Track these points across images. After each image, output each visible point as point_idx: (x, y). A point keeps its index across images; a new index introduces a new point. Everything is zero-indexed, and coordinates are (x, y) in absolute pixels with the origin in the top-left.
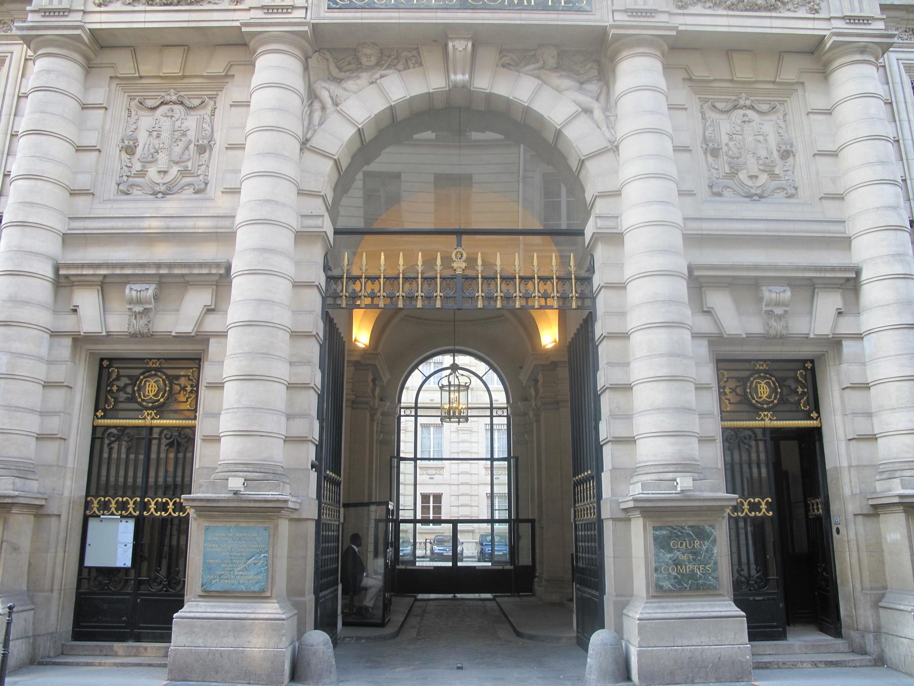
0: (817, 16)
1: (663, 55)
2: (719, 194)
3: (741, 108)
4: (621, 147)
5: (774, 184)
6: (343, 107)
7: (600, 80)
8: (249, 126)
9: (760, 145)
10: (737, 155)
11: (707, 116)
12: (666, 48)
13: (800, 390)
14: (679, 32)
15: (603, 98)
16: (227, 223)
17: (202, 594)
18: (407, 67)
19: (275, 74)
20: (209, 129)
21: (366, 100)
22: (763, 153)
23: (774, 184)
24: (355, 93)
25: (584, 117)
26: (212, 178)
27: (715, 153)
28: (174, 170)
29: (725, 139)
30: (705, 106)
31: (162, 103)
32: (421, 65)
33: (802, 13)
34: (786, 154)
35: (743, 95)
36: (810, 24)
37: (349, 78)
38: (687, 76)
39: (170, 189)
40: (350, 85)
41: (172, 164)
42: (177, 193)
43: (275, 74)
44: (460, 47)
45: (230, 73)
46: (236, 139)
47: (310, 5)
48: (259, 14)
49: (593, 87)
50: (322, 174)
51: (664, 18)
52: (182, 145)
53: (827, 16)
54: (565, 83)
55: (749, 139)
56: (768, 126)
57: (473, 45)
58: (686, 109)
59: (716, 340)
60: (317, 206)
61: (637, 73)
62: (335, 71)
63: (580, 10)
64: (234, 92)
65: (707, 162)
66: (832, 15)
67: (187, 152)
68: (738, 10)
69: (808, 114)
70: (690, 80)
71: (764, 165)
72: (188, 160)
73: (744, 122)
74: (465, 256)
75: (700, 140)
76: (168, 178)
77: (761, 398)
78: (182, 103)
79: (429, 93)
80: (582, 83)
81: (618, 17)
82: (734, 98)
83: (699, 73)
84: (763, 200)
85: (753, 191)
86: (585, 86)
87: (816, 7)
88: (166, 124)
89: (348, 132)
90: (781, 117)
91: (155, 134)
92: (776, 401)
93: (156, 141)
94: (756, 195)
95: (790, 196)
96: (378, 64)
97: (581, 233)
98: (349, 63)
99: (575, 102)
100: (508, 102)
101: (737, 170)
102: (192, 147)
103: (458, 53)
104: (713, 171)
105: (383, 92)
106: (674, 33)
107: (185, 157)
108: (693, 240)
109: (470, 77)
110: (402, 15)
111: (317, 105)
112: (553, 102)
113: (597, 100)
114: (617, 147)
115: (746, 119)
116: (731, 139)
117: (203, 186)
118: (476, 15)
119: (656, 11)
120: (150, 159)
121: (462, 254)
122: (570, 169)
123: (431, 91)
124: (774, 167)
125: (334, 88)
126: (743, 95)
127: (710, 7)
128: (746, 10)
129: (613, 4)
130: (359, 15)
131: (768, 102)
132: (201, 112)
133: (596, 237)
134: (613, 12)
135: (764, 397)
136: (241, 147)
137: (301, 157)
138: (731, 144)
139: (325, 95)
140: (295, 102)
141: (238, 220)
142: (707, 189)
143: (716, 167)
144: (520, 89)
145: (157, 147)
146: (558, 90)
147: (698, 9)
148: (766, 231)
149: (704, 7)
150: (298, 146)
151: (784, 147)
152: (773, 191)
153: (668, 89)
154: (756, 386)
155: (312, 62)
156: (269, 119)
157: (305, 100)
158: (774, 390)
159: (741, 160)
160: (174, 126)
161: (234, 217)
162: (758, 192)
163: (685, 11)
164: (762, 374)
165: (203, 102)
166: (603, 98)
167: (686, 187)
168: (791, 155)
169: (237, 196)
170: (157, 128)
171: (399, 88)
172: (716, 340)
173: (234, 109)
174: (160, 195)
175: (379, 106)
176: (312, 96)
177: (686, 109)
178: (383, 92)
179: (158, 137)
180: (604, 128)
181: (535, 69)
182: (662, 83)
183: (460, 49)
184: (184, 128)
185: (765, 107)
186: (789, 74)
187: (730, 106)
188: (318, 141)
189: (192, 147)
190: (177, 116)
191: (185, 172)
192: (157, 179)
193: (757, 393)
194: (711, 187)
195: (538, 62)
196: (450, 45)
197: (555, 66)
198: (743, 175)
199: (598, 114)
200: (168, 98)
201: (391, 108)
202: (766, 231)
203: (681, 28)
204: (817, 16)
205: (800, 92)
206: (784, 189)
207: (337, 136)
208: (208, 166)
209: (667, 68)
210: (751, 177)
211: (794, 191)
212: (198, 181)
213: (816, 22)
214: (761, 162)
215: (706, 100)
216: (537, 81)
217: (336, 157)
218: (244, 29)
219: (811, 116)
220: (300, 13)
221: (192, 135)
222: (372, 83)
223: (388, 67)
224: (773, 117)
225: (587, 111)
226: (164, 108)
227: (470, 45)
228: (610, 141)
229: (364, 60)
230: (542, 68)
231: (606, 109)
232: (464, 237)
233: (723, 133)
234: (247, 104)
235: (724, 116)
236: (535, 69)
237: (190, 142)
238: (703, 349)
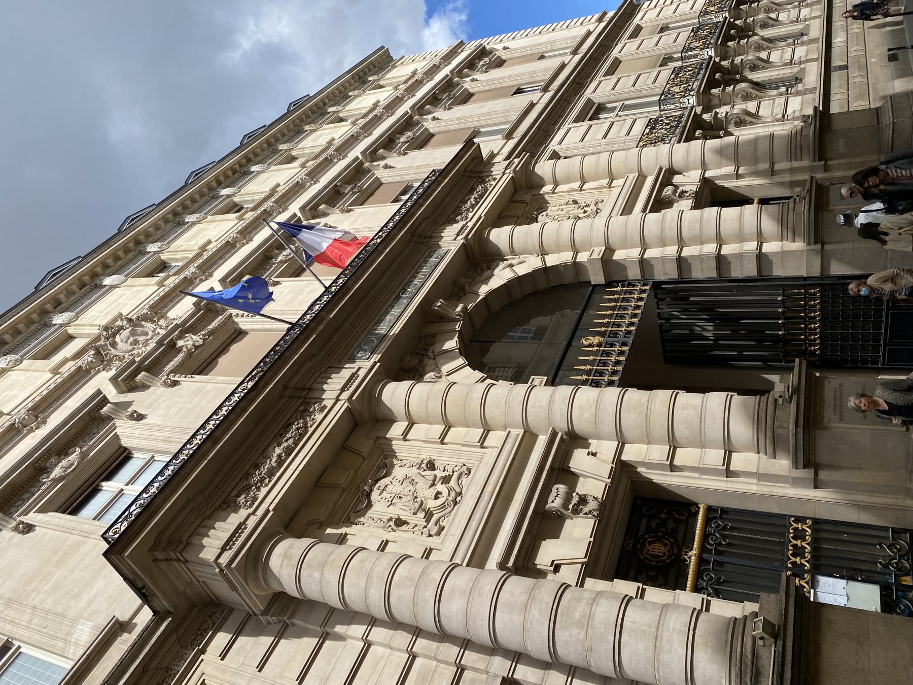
3: (371, 490)
5: (453, 482)
13: (663, 516)
17: (21, 650)
27: (400, 523)
38: (317, 525)
56: (398, 472)
59: (594, 567)
77: (664, 553)
82: (359, 494)
92: (672, 540)
95: (469, 470)
104: (416, 529)
106: (271, 513)
127: (270, 481)
135: (663, 550)
151: (424, 466)
154: (651, 555)
158: (659, 540)
162: (453, 494)
163: (259, 500)
164: (639, 546)
172: (594, 567)
182: (306, 542)
193: (660, 556)
194: (430, 535)
210: (436, 498)
238: (593, 584)
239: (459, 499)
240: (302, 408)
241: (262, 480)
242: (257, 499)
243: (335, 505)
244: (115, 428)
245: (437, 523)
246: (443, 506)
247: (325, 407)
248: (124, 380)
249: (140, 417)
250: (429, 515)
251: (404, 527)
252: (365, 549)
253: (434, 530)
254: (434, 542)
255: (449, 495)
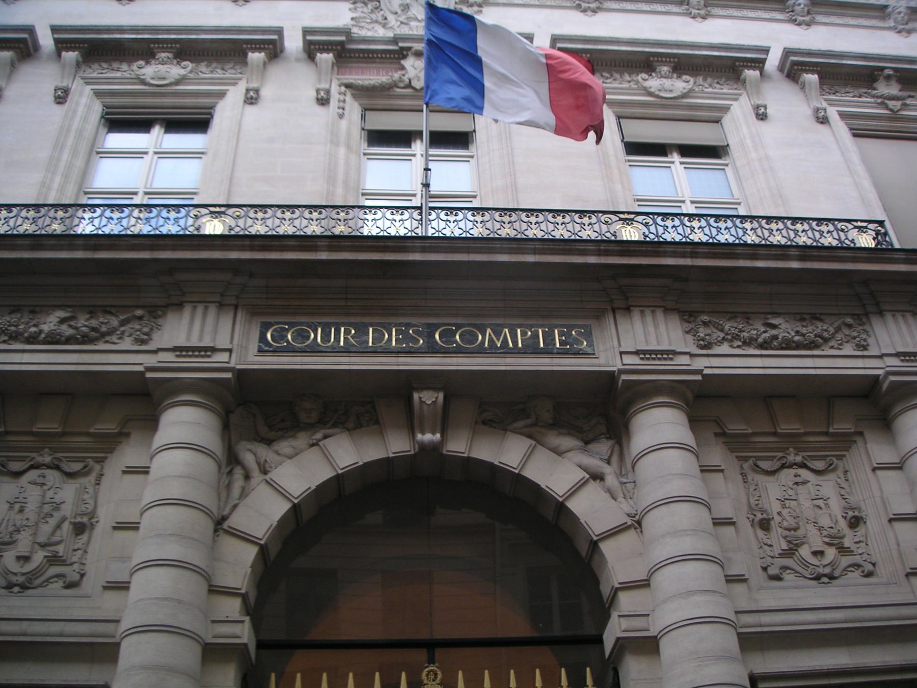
0: (866, 353)
1: (687, 405)
2: (777, 578)
3: (790, 467)
4: (644, 524)
5: (845, 561)
6: (273, 475)
7: (609, 438)
8: (147, 498)
9: (820, 512)
10: (794, 525)
11: (750, 478)
12: (690, 396)
14: (705, 376)
15: (615, 459)
16: (109, 628)
18: (359, 426)
19: (185, 425)
20: (92, 502)
21: (301, 470)
22: (825, 522)
23: (845, 561)
24: (290, 458)
25: (593, 486)
26: (90, 569)
27: (765, 525)
28: (39, 557)
29: (776, 507)
30: (746, 465)
31: (32, 467)
32: (377, 422)
33: (848, 350)
34: (855, 522)
35: (791, 449)
36: (859, 363)
37: (282, 438)
38: (719, 431)
39: (30, 581)
40: (285, 446)
41: (37, 547)
42: (40, 586)
43: (185, 425)
44: (428, 398)
45: (125, 431)
46: (130, 515)
47: (235, 347)
48: (170, 357)
49: (604, 447)
50: (238, 565)
51: (683, 361)
52: (53, 522)
53: (878, 353)
54: (567, 442)
55: (806, 504)
56: (828, 486)
57: (445, 397)
58: (722, 471)
60: (232, 607)
61: (659, 427)
62: (263, 430)
63: (578, 353)
64: (129, 454)
65: (757, 537)
66: (884, 351)
67: (58, 533)
68: (772, 349)
69: (874, 469)
70: (724, 434)
71: (830, 536)
72: (59, 543)
73: (796, 483)
74: (439, 677)
75: (745, 508)
76: (29, 567)
78: (57, 468)
79: (388, 458)
80: (587, 443)
81: (628, 359)
82: (780, 454)
83: (736, 427)
84: (835, 582)
85: (821, 570)
86: (590, 446)
87: (863, 343)
88: (33, 495)
89: (281, 508)
90: (842, 475)
91: (17, 506)
93: (19, 517)
94: (825, 575)
95: (869, 574)
96: (322, 422)
97: (599, 640)
98: (283, 421)
99: (580, 467)
100: (491, 467)
101: (798, 545)
102: (66, 526)
103: (425, 407)
104: (766, 548)
105: (328, 459)
106: (699, 378)
107: (56, 538)
108: (752, 642)
109: (442, 436)
110: (353, 359)
111: (238, 472)
112: (555, 470)
113: (609, 462)
114: (639, 523)
115: (798, 479)
116: (784, 507)
117: (77, 577)
118: (448, 360)
119: (675, 353)
120: (7, 539)
121: (436, 675)
122: (577, 553)
123: (391, 455)
124: (843, 537)
125: (263, 452)
126: (791, 449)
127: (739, 347)
128: (782, 349)
129: (620, 345)
130: (298, 359)
131: (823, 458)
132: (84, 481)
133: (622, 645)
134: (621, 353)
136: (134, 527)
137: (214, 541)
138: (785, 512)
139: (249, 459)
140: (208, 466)
141: (125, 625)
142: (760, 571)
143: (769, 542)
144: (509, 453)
145: (18, 523)
146: (559, 452)
147: (725, 349)
148: (846, 622)
149: (731, 346)
150: (211, 526)
151: (851, 514)
152: (845, 570)
153: (698, 446)
155: (234, 419)
156: (175, 490)
157: (224, 463)
159: (800, 533)
160: (43, 496)
161: (118, 621)
162: (827, 570)
163: (709, 352)
165: (85, 467)
166: (615, 459)
167: (734, 571)
168: (861, 522)
169: (124, 592)
170: (21, 500)
171: (347, 453)
173: (128, 477)
174: (16, 589)
175: (324, 474)
176: (232, 460)
177: (722, 471)
178: (328, 459)
179: (21, 511)
180: (621, 499)
181: (526, 427)
182: (688, 438)
183: (429, 402)
184: (58, 499)
185: (820, 465)
186: (842, 426)
187: (777, 465)
188: (238, 520)
189: (66, 526)
190: (49, 484)
191: (54, 560)
192: (15, 567)
194: (765, 569)
195: (528, 417)
196: (416, 396)
197: (551, 422)
198: (805, 552)
199: (611, 480)
200: (40, 459)
201: (338, 478)
202: (846, 622)
203: (706, 371)
204: (866, 353)
205: (860, 443)
206: (858, 566)
207: (263, 512)
208: (86, 552)
209: (694, 422)
210: (815, 553)
211: (871, 567)
212: (71, 573)
213: (866, 360)
214: (825, 533)
215: (746, 459)
216: (529, 442)
217: (243, 591)
218: (149, 375)
219: (879, 472)
220: (223, 357)
221: (67, 510)
222: (312, 445)
223: (335, 425)
224: (832, 476)
225: (597, 477)
226: (33, 475)
227: (441, 396)
228: (628, 515)
229: (303, 417)
230: (535, 425)
231: (620, 474)
232: (439, 652)
233: (773, 499)
234: (145, 471)
235: (770, 478)
236: (526, 427)
237: (64, 519)
239: (825, 580)
240: (849, 320)
241: (736, 337)
242: (710, 349)
243: (754, 434)
244: (736, 100)
245: (785, 568)
246: (805, 563)
247: (865, 348)
248: (794, 63)
249: (762, 117)
250: (790, 552)
251: (760, 533)
252: (710, 510)
253: (773, 571)
254: (757, 577)
255: (825, 566)
